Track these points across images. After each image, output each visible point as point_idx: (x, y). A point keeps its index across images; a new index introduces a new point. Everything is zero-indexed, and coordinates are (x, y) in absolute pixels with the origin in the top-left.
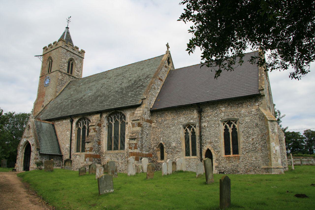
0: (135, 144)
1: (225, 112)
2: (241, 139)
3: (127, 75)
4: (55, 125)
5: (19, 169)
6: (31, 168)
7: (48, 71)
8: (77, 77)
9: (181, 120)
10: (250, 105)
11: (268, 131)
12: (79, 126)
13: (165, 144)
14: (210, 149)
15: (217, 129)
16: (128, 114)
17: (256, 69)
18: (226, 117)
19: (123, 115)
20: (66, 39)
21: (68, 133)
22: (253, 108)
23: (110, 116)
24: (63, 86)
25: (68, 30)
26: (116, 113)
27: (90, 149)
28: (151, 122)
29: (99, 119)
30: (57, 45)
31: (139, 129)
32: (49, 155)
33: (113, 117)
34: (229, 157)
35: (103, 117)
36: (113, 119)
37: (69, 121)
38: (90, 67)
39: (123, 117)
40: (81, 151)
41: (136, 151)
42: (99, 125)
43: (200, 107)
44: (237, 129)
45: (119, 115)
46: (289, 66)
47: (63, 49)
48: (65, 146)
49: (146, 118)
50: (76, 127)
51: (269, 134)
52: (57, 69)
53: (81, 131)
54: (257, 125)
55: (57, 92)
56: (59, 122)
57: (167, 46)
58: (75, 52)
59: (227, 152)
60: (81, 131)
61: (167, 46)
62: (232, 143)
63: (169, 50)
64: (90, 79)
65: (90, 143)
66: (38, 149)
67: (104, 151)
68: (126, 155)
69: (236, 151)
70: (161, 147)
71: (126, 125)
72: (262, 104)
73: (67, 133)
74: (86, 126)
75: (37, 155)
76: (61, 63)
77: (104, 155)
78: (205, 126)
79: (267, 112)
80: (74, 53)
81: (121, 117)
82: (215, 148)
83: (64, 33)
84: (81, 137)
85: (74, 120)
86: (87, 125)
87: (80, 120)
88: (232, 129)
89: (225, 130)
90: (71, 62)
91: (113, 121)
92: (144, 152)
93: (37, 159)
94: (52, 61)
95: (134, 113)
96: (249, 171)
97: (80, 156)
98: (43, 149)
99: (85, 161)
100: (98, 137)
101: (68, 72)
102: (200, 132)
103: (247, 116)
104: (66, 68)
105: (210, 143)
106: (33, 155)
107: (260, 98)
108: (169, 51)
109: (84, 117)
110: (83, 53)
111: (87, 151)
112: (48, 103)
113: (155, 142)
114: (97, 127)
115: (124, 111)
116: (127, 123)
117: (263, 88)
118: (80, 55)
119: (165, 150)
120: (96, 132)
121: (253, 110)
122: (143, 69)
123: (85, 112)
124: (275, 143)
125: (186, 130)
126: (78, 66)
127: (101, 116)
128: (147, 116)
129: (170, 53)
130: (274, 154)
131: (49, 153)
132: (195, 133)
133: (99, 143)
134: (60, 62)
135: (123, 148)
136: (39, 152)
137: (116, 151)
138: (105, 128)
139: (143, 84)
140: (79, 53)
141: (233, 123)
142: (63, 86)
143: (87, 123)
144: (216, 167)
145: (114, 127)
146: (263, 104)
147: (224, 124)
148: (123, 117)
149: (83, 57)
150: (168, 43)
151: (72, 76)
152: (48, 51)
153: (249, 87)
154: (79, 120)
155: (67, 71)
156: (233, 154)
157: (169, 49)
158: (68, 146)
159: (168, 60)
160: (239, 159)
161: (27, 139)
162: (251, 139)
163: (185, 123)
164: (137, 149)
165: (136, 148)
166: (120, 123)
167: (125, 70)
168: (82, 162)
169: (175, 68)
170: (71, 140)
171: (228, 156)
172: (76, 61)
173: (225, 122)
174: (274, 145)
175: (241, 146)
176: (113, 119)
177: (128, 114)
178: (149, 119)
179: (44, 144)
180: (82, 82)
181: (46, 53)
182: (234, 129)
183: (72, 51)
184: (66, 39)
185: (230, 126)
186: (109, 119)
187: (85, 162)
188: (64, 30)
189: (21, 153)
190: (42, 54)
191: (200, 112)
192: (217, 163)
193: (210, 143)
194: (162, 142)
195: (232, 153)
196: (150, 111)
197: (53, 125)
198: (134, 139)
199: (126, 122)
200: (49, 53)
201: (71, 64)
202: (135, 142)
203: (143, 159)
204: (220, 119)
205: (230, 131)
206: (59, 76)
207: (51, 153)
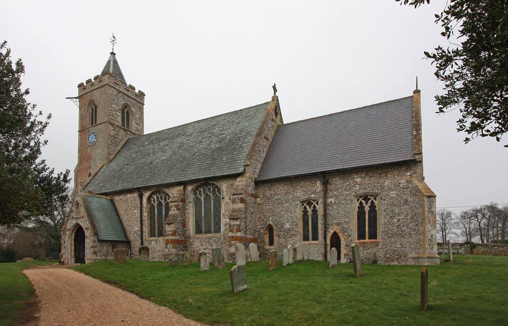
0: (237, 225)
1: (360, 184)
2: (381, 221)
3: (216, 130)
4: (114, 201)
5: (68, 262)
6: (88, 259)
7: (91, 122)
8: (136, 133)
9: (298, 194)
10: (398, 174)
11: (424, 209)
12: (152, 202)
13: (276, 226)
14: (337, 232)
15: (348, 206)
16: (224, 186)
17: (409, 124)
18: (362, 191)
19: (217, 187)
20: (113, 72)
21: (137, 212)
22: (402, 179)
23: (197, 188)
24: (118, 145)
25: (114, 58)
26: (207, 183)
27: (173, 232)
28: (255, 196)
29: (183, 193)
30: (101, 81)
31: (242, 205)
32: (112, 241)
33: (202, 190)
34: (364, 242)
35: (187, 190)
36: (202, 193)
37: (135, 195)
38: (156, 119)
39: (216, 190)
40: (157, 235)
41: (239, 234)
42: (183, 201)
43: (325, 177)
44: (377, 206)
45: (211, 188)
46: (495, 123)
47: (112, 89)
48: (133, 228)
49: (250, 192)
50: (148, 204)
51: (424, 214)
52: (106, 120)
53: (156, 209)
54: (406, 202)
56: (121, 197)
57: (274, 87)
58: (130, 94)
59: (361, 236)
60: (156, 209)
61: (274, 87)
62: (368, 224)
63: (277, 95)
64: (159, 136)
65: (172, 225)
66: (96, 234)
67: (192, 235)
68: (222, 240)
69: (373, 235)
70: (270, 229)
71: (222, 201)
72: (416, 173)
73: (135, 211)
74: (163, 202)
75: (94, 242)
76: (111, 110)
77: (191, 241)
78: (331, 202)
79: (422, 185)
81: (214, 189)
82: (344, 231)
83: (109, 62)
84: (156, 217)
85: (144, 194)
86: (164, 200)
87: (153, 193)
88: (370, 207)
89: (359, 207)
90: (126, 110)
91: (203, 194)
92: (249, 236)
93: (96, 247)
94: (96, 107)
95: (232, 185)
96: (390, 261)
97: (156, 242)
98: (103, 234)
99: (167, 248)
100: (182, 217)
101: (123, 125)
102: (325, 210)
103: (393, 190)
104: (119, 119)
105: (338, 224)
106: (89, 242)
107: (414, 164)
108: (277, 97)
109: (159, 189)
110: (142, 96)
111: (168, 235)
112: (99, 171)
113: (262, 223)
114: (181, 204)
115: (219, 181)
116: (223, 198)
117: (419, 151)
118: (138, 99)
119: (275, 233)
120: (180, 210)
121: (402, 181)
122: (239, 123)
123: (161, 183)
124: (431, 226)
125: (305, 208)
127: (185, 188)
128: (251, 190)
129: (278, 100)
130: (429, 240)
131: (111, 239)
132: (317, 211)
133: (184, 225)
134: (109, 110)
135: (218, 230)
136: (98, 238)
137: (209, 235)
138: (191, 205)
139: (242, 144)
141: (372, 198)
142: (118, 145)
143: (163, 197)
144: (345, 255)
146: (417, 173)
147: (358, 200)
148: (216, 190)
149: (142, 102)
150: (275, 84)
151: (129, 131)
152: (87, 91)
153: (399, 150)
154: (151, 194)
155: (121, 124)
156: (369, 239)
157: (277, 94)
158: (137, 228)
159: (276, 110)
160: (378, 246)
161: (76, 221)
162: (395, 220)
163: (304, 198)
164: (240, 232)
165: (238, 230)
166: (213, 198)
167: (212, 123)
168: (160, 250)
169: (284, 123)
170: (142, 221)
171: (362, 241)
172: (133, 109)
173: (361, 197)
174: (430, 229)
175: (380, 229)
176: (202, 193)
177: (224, 186)
178: (254, 193)
179: (103, 227)
180: (147, 140)
181: (84, 94)
182: (373, 206)
183: (125, 92)
184: (113, 72)
185: (367, 203)
186: (196, 192)
187: (167, 250)
189: (70, 240)
190: (77, 95)
191: (325, 184)
192: (347, 249)
193: (338, 224)
194: (271, 223)
195: (367, 237)
196: (255, 182)
197: (112, 201)
198: (237, 219)
199: (221, 197)
200: (89, 94)
201: (126, 113)
202: (237, 223)
203: (251, 244)
204: (354, 194)
205: (367, 209)
206: (111, 131)
207: (114, 239)
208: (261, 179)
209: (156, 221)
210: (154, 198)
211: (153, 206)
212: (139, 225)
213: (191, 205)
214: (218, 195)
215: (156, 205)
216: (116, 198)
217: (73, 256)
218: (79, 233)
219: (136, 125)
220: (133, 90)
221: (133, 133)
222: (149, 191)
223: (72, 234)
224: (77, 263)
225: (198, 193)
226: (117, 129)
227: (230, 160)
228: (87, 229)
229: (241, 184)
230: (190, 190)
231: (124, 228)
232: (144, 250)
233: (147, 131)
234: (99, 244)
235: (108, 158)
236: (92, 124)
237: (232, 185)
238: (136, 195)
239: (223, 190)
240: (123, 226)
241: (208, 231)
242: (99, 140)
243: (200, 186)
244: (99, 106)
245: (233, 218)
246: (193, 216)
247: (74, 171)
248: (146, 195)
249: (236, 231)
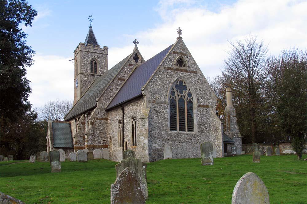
47: (84, 52)
55: (82, 93)
80: (95, 53)
90: (94, 62)
104: (89, 69)
114: (81, 125)
126: (102, 64)
140: (101, 50)
145: (176, 116)
174: (143, 139)
188: (88, 30)
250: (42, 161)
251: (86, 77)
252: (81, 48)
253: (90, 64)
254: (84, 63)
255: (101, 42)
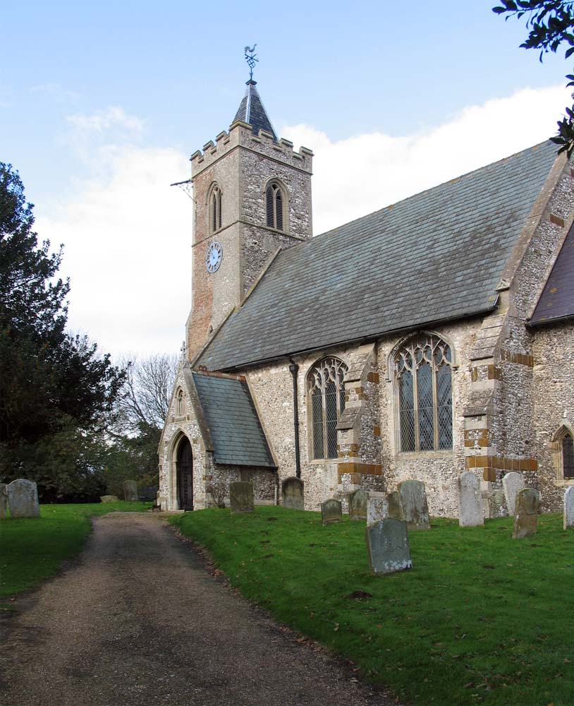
8: (297, 236)
12: (317, 383)
19: (442, 343)
21: (288, 404)
23: (402, 348)
25: (252, 90)
26: (421, 334)
27: (352, 448)
33: (321, 372)
39: (442, 349)
42: (374, 378)
45: (431, 346)
47: (248, 154)
48: (281, 441)
50: (309, 387)
56: (260, 375)
65: (349, 431)
67: (393, 453)
68: (456, 464)
71: (454, 376)
73: (285, 404)
77: (392, 467)
81: (437, 349)
83: (244, 100)
84: (325, 415)
85: (301, 366)
86: (337, 377)
87: (316, 365)
90: (275, 192)
91: (414, 363)
92: (512, 456)
94: (220, 194)
100: (372, 414)
101: (270, 222)
104: (262, 212)
111: (343, 455)
112: (225, 323)
113: (546, 423)
114: (368, 384)
116: (456, 368)
118: (299, 166)
127: (376, 350)
128: (515, 345)
131: (239, 463)
133: (377, 432)
135: (446, 443)
136: (214, 460)
137: (428, 454)
148: (442, 349)
151: (282, 234)
152: (205, 165)
155: (265, 222)
158: (289, 440)
161: (178, 427)
164: (489, 445)
170: (297, 424)
176: (413, 357)
177: (457, 339)
178: (524, 352)
180: (314, 250)
183: (273, 155)
188: (244, 91)
190: (189, 177)
196: (527, 327)
197: (244, 384)
199: (452, 365)
206: (246, 239)
208: (543, 319)
209: (325, 424)
210: (319, 375)
211: (317, 391)
212: (293, 433)
213: (390, 386)
214: (447, 362)
215: (323, 391)
216: (252, 378)
217: (175, 495)
218: (183, 445)
219: (296, 220)
220: (288, 149)
221: (290, 237)
222: (310, 359)
223: (173, 450)
224: (181, 509)
225: (404, 358)
226: (258, 234)
227: (470, 281)
228: (195, 441)
229: (490, 335)
230: (387, 353)
231: (265, 440)
232: (296, 483)
233: (323, 222)
234: (217, 472)
235: (242, 296)
236: (215, 230)
237: (474, 336)
238: (285, 369)
239: (455, 350)
240: (264, 436)
241: (427, 445)
242: (225, 259)
243: (406, 344)
244: (225, 192)
245: (473, 413)
246: (395, 411)
247: (186, 325)
248: (305, 367)
249: (478, 444)
250: (410, 523)
251: (254, 234)
252: (242, 139)
253: (265, 196)
254: (248, 191)
255: (292, 130)
